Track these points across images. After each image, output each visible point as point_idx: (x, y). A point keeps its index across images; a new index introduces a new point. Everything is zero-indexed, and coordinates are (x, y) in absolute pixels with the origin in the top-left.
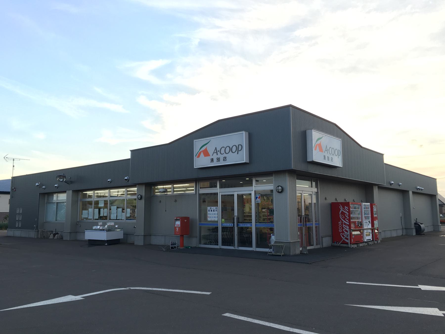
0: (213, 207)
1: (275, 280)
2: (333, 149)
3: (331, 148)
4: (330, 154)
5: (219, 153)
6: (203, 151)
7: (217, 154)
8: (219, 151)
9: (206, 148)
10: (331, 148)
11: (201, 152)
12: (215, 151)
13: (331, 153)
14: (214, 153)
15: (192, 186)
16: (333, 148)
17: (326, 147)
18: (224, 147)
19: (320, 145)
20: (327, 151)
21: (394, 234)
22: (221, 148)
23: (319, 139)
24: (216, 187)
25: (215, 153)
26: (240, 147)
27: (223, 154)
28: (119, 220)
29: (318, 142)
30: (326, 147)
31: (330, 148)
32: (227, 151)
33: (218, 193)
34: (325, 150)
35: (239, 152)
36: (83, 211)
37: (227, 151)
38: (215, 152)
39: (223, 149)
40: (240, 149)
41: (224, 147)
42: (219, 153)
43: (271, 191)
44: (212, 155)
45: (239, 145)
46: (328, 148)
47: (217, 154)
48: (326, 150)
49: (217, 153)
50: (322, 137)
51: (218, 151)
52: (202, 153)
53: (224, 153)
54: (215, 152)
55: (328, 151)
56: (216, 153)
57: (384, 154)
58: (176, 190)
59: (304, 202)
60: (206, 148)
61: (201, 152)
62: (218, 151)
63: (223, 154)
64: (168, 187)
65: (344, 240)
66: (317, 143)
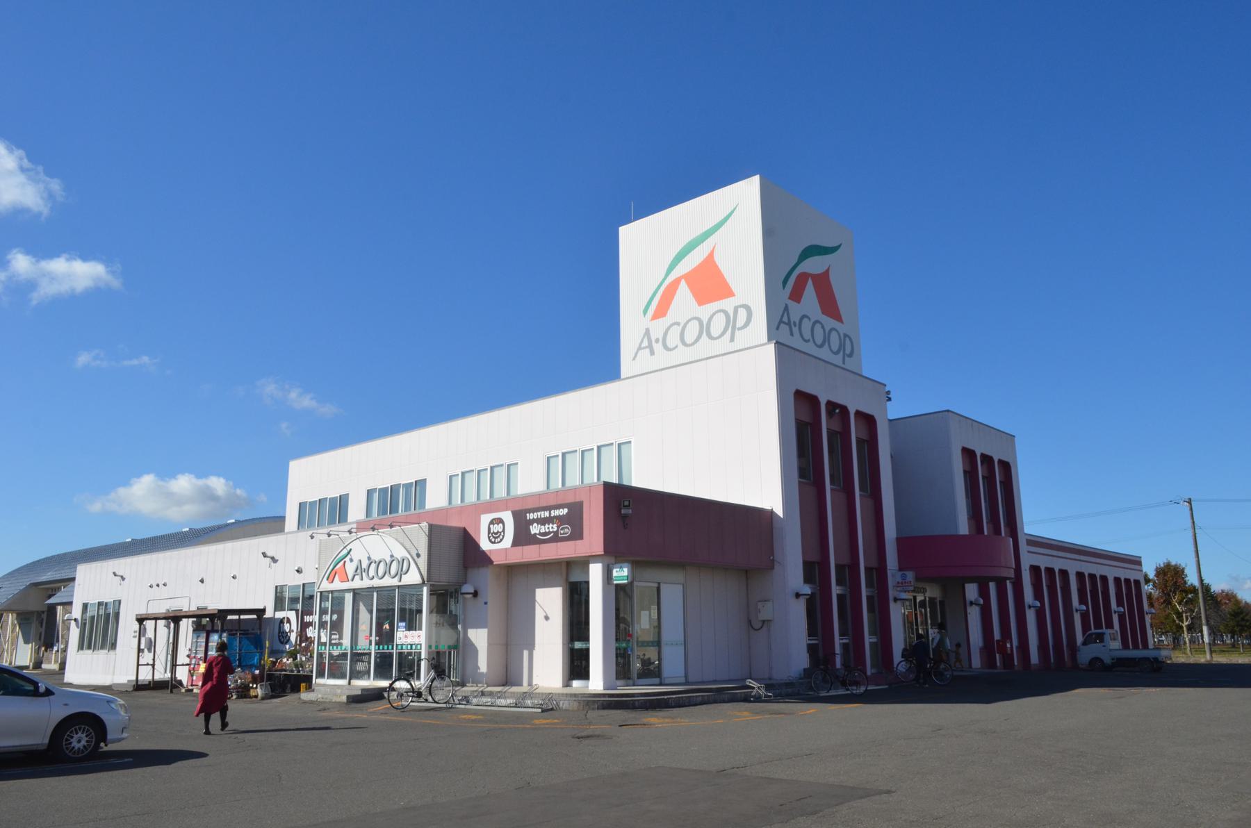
1: (798, 800)
5: (658, 347)
6: (690, 278)
7: (652, 353)
9: (711, 254)
10: (809, 319)
11: (676, 283)
12: (645, 343)
13: (807, 335)
14: (640, 348)
18: (678, 324)
20: (789, 324)
21: (418, 583)
24: (51, 663)
25: (644, 348)
26: (742, 314)
27: (677, 347)
28: (154, 660)
29: (814, 265)
32: (689, 338)
33: (81, 647)
35: (737, 333)
38: (643, 346)
39: (675, 332)
40: (740, 323)
41: (678, 324)
42: (658, 347)
43: (82, 649)
44: (634, 359)
45: (736, 309)
47: (652, 353)
48: (785, 319)
49: (650, 347)
52: (683, 287)
53: (680, 345)
54: (643, 346)
55: (795, 330)
56: (647, 350)
58: (623, 580)
59: (169, 633)
60: (711, 254)
61: (676, 283)
63: (677, 347)
64: (986, 510)
65: (284, 610)
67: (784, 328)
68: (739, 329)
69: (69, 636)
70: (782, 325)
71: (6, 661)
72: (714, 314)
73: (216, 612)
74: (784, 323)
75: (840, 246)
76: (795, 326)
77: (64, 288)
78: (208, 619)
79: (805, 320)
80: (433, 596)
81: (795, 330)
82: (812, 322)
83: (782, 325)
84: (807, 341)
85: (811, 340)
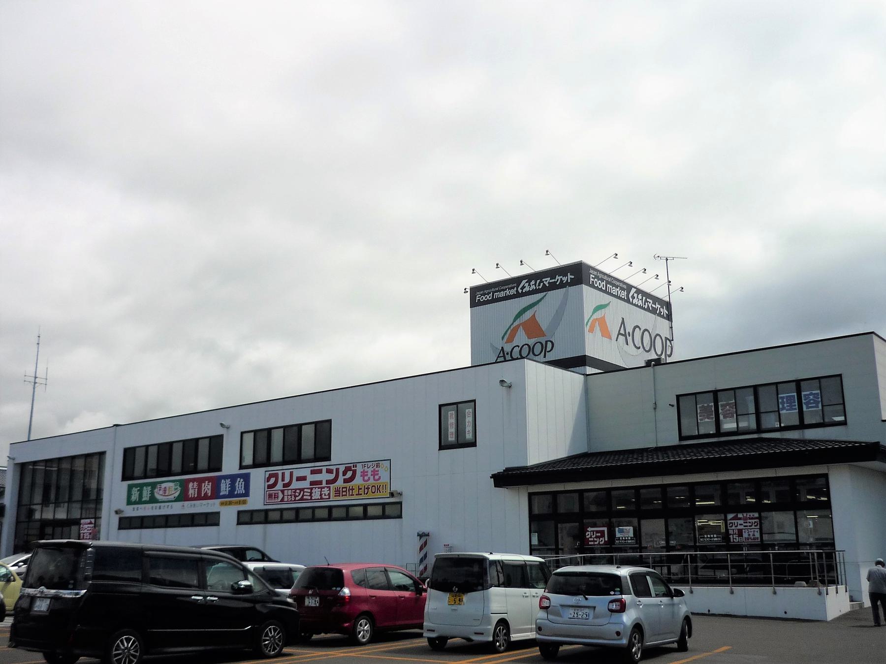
0: (664, 483)
2: (646, 333)
3: (640, 329)
4: (639, 348)
8: (509, 354)
10: (640, 329)
13: (639, 344)
15: (134, 533)
16: (646, 330)
17: (623, 322)
18: (519, 346)
19: (602, 322)
20: (625, 335)
22: (552, 351)
23: (599, 308)
26: (549, 345)
29: (598, 315)
30: (623, 322)
31: (637, 329)
34: (619, 334)
36: (362, 507)
37: (524, 354)
39: (517, 350)
40: (548, 349)
41: (519, 346)
45: (546, 342)
46: (629, 329)
48: (622, 331)
50: (608, 303)
51: (508, 354)
55: (630, 339)
57: (220, 512)
61: (518, 326)
62: (508, 354)
66: (540, 297)
67: (621, 338)
68: (548, 352)
69: (219, 521)
70: (620, 336)
71: (723, 529)
72: (536, 344)
73: (101, 498)
74: (622, 335)
75: (609, 304)
76: (629, 336)
77: (207, 572)
78: (633, 491)
79: (637, 329)
80: (533, 553)
81: (630, 339)
82: (642, 331)
83: (620, 336)
84: (639, 348)
85: (641, 347)
